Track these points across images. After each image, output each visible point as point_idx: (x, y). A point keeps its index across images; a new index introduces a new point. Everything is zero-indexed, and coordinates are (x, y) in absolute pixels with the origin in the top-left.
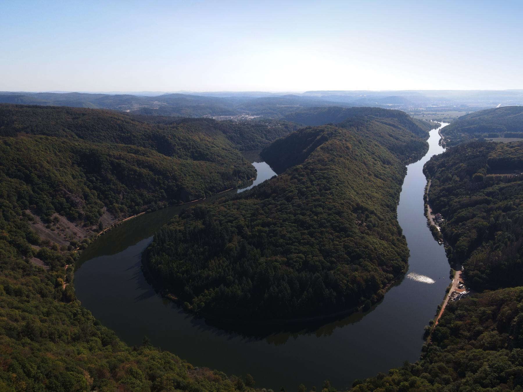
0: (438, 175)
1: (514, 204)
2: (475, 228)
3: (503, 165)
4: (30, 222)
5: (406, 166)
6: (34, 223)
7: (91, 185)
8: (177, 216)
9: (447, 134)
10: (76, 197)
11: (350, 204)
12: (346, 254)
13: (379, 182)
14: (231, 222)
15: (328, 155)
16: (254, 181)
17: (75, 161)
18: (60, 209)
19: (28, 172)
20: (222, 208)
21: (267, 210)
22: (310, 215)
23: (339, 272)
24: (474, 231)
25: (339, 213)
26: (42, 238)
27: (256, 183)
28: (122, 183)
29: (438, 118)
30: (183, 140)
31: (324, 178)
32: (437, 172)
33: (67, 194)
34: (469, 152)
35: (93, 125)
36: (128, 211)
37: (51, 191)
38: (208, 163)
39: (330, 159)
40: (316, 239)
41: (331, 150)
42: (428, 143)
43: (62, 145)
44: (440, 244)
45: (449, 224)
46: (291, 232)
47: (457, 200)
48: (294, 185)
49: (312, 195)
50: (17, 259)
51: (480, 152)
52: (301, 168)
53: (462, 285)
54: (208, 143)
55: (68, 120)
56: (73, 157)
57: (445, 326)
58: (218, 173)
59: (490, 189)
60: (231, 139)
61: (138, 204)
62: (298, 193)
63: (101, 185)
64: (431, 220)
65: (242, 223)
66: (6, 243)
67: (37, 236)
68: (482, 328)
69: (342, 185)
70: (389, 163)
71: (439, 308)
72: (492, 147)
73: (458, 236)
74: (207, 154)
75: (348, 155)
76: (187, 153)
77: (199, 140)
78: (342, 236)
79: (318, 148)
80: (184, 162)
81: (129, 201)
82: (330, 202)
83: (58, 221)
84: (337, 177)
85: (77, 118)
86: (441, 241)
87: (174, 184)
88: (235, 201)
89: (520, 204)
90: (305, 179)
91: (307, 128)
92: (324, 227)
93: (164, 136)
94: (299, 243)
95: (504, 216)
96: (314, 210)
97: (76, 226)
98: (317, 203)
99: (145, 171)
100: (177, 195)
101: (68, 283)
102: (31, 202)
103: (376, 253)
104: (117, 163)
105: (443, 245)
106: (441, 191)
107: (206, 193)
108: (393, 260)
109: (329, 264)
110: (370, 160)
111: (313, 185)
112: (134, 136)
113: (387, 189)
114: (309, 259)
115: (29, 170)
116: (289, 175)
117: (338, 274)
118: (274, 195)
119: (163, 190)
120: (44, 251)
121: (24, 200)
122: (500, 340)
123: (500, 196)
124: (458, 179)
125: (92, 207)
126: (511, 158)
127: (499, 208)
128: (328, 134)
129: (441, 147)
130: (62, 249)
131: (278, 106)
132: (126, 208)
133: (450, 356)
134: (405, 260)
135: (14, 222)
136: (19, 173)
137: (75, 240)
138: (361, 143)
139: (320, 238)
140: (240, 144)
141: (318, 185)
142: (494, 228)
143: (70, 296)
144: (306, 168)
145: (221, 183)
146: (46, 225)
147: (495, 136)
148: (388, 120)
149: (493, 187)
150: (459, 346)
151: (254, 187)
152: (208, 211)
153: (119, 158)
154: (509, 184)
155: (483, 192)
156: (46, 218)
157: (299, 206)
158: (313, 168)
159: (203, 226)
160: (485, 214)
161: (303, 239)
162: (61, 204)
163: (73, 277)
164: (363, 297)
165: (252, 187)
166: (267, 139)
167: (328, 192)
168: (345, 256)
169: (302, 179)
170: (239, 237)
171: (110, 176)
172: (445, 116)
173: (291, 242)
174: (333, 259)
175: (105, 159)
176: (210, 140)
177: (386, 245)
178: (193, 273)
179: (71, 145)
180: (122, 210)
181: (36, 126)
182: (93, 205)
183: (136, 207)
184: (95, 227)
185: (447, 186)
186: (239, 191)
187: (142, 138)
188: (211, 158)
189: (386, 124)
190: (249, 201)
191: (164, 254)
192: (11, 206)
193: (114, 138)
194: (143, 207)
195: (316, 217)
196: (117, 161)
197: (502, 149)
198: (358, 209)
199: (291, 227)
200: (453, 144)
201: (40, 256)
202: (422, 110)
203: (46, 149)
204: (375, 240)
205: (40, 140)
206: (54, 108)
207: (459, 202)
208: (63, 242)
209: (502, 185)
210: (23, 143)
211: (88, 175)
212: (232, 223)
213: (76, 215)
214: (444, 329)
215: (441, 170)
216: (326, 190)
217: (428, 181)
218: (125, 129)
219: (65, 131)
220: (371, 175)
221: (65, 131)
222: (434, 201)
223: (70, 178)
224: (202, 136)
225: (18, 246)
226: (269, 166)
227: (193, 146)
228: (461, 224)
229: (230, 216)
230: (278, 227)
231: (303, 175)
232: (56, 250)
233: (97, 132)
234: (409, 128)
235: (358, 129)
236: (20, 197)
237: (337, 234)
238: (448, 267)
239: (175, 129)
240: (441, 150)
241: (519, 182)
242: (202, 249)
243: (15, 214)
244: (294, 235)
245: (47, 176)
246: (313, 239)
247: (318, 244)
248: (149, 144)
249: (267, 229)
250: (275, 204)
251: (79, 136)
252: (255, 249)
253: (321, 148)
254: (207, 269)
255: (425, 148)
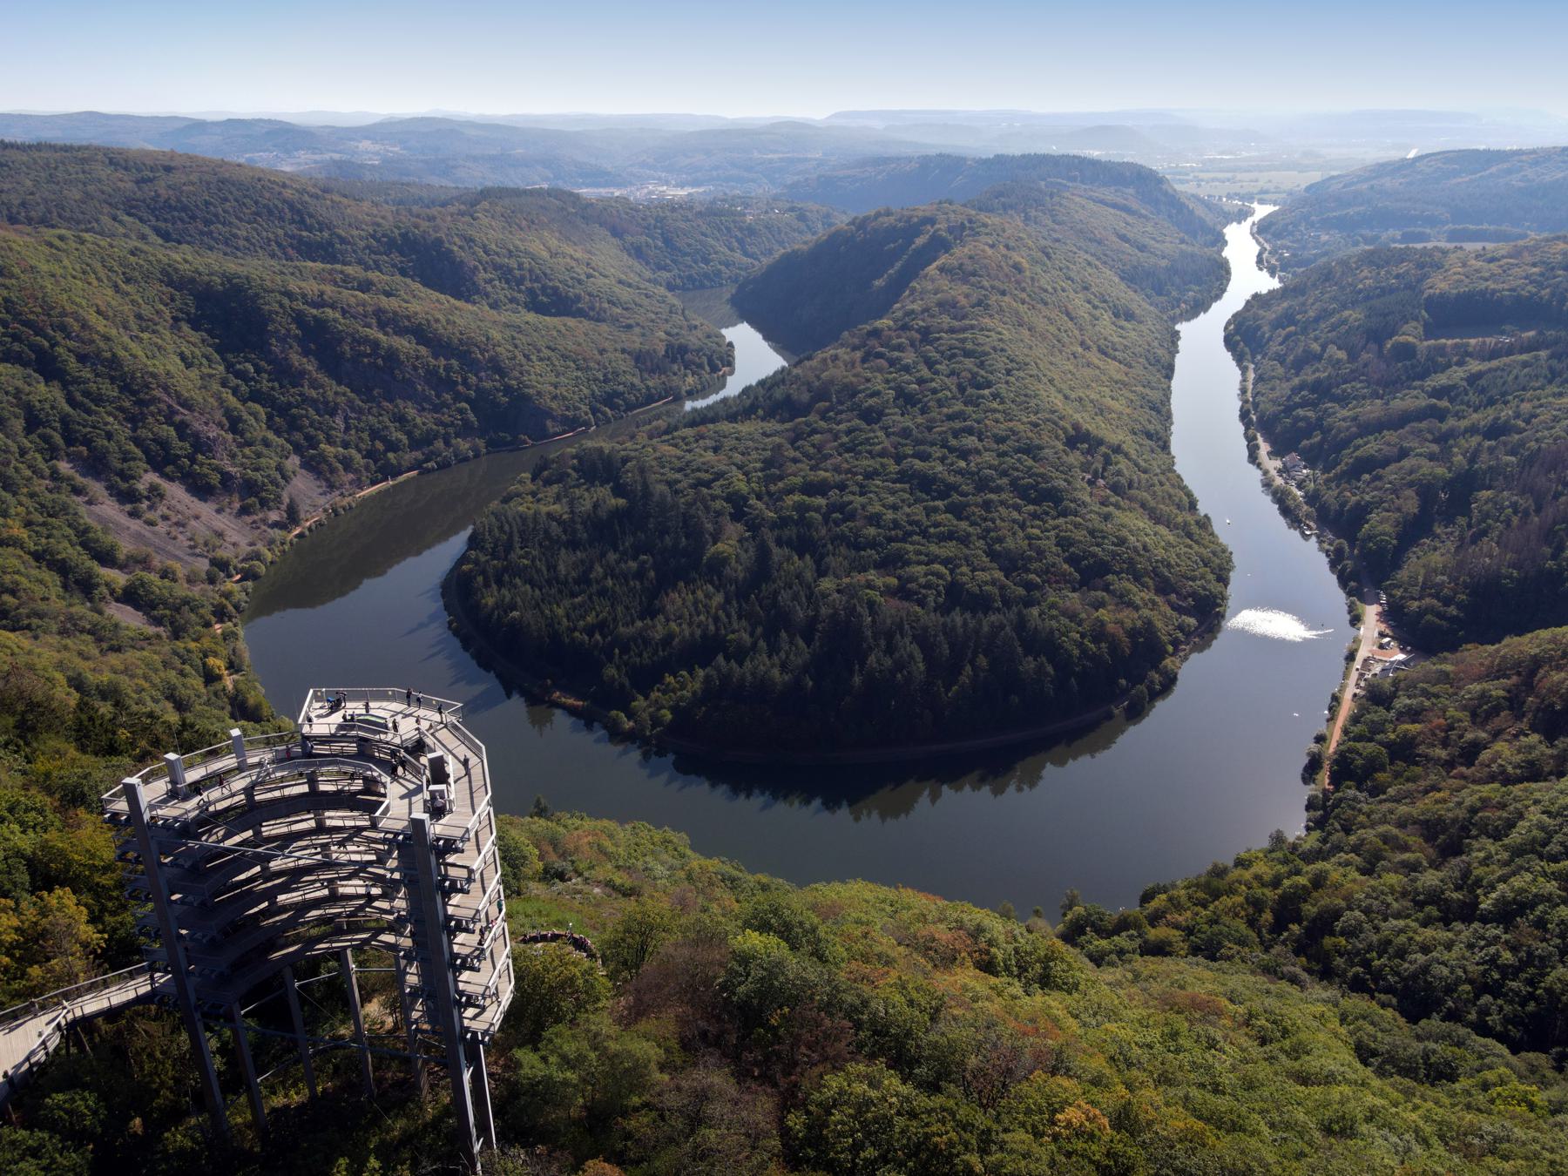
0: (1274, 347)
1: (1517, 416)
2: (1410, 485)
3: (1469, 312)
4: (79, 499)
5: (1178, 327)
6: (90, 503)
7: (244, 388)
8: (527, 475)
9: (1278, 236)
10: (206, 424)
11: (1055, 423)
12: (1066, 560)
13: (1113, 367)
14: (708, 484)
15: (965, 288)
16: (729, 379)
17: (181, 310)
18: (161, 460)
19: (46, 344)
20: (666, 448)
21: (812, 450)
22: (942, 460)
23: (1054, 612)
24: (1410, 492)
25: (1030, 450)
26: (125, 548)
27: (734, 386)
28: (339, 383)
29: (1242, 191)
30: (497, 254)
31: (968, 354)
32: (1270, 339)
33: (177, 413)
34: (1367, 278)
35: (207, 203)
36: (367, 468)
37: (127, 404)
38: (586, 325)
39: (974, 299)
40: (972, 524)
41: (974, 274)
42: (1226, 262)
43: (132, 258)
44: (1306, 537)
45: (1327, 481)
46: (895, 508)
47: (1345, 413)
48: (879, 377)
49: (939, 401)
50: (71, 605)
51: (1397, 277)
52: (890, 329)
53: (1387, 640)
54: (574, 264)
55: (120, 184)
56: (173, 300)
57: (1370, 740)
58: (623, 351)
59: (1441, 380)
60: (638, 252)
61: (393, 446)
62: (896, 399)
63: (273, 389)
64: (1273, 473)
65: (743, 487)
66: (27, 557)
67: (110, 538)
68: (1484, 735)
69: (1022, 374)
70: (1129, 316)
71: (1336, 699)
72: (1431, 263)
73: (1361, 513)
74: (578, 298)
75: (1023, 290)
76: (518, 296)
77: (545, 254)
78: (1047, 514)
79: (932, 269)
80: (515, 319)
81: (365, 436)
82: (997, 421)
83: (162, 496)
84: (1002, 350)
85: (151, 180)
86: (1310, 528)
87: (497, 384)
88: (702, 428)
89: (1536, 416)
90: (909, 357)
91: (878, 215)
92: (992, 491)
93: (439, 241)
94: (924, 533)
95: (1491, 450)
96: (953, 442)
97: (219, 511)
98: (958, 425)
99: (404, 344)
100: (508, 419)
101: (237, 672)
102: (69, 441)
103: (1149, 559)
104: (314, 317)
105: (1314, 539)
106: (1296, 390)
107: (594, 411)
108: (1193, 579)
109: (1021, 591)
110: (1079, 304)
111: (937, 373)
112: (343, 241)
113: (1139, 389)
114: (964, 579)
115: (46, 337)
116: (855, 348)
117: (1053, 617)
118: (822, 405)
119: (464, 405)
120: (143, 584)
121: (48, 431)
122: (1552, 757)
123: (1473, 397)
124: (1342, 355)
125: (259, 455)
126: (1494, 292)
127: (1473, 430)
128: (950, 230)
129: (1265, 273)
130: (190, 581)
131: (756, 155)
132: (357, 457)
133: (1403, 809)
134: (1223, 580)
135: (32, 495)
136: (16, 347)
137: (224, 553)
138: (1049, 258)
139: (985, 520)
140: (665, 268)
141: (952, 373)
142: (1464, 487)
143: (258, 707)
144: (905, 327)
145: (636, 381)
146: (128, 507)
147: (1422, 237)
148: (1108, 194)
149: (1449, 372)
150: (1423, 784)
151: (724, 400)
152: (625, 460)
153: (320, 303)
154: (1494, 363)
155: (1422, 388)
156: (124, 486)
157: (905, 433)
158: (927, 328)
159: (621, 502)
160: (1435, 448)
161: (936, 525)
162: (164, 444)
163: (247, 656)
164: (1114, 683)
165: (712, 399)
166: (746, 254)
167: (986, 392)
168: (1066, 566)
169: (899, 359)
170: (740, 527)
171: (296, 359)
172: (1261, 184)
173: (900, 533)
174: (1032, 576)
175: (276, 307)
176: (578, 255)
177: (1171, 538)
178: (622, 629)
179: (159, 261)
180: (347, 464)
181: (23, 204)
182: (260, 448)
183: (391, 455)
184: (274, 516)
185: (1309, 375)
186: (689, 405)
187: (367, 247)
188: (592, 309)
189: (1102, 202)
190: (745, 428)
191: (518, 581)
192: (14, 448)
193: (279, 245)
194: (410, 457)
195: (963, 464)
196: (314, 311)
197: (1464, 265)
198: (1077, 438)
199: (893, 493)
200: (1300, 264)
201: (130, 597)
202: (1193, 169)
203: (84, 273)
204: (1141, 525)
205: (57, 242)
206: (66, 149)
207: (1355, 419)
208: (190, 559)
209: (1475, 366)
210: (11, 249)
211: (230, 356)
212: (709, 487)
213: (215, 479)
214: (1369, 748)
215: (1284, 333)
216: (979, 387)
217: (1244, 370)
218: (311, 216)
219: (120, 222)
220: (1088, 348)
221: (120, 222)
222: (1272, 425)
223: (176, 362)
224: (553, 243)
225: (62, 568)
226: (760, 336)
227: (531, 271)
228: (1366, 477)
229: (699, 470)
230: (854, 494)
231: (900, 348)
232: (175, 580)
233: (224, 224)
234: (1170, 216)
235: (1027, 219)
236: (33, 422)
237: (1031, 508)
238: (1340, 597)
239: (467, 219)
240: (1267, 283)
241: (1524, 357)
242: (633, 565)
243: (28, 473)
244: (908, 515)
245: (108, 355)
246: (964, 525)
247: (984, 538)
248: (394, 266)
249: (820, 501)
250: (830, 430)
251: (166, 236)
252: (796, 558)
253: (941, 269)
254: (661, 617)
255: (1217, 276)
